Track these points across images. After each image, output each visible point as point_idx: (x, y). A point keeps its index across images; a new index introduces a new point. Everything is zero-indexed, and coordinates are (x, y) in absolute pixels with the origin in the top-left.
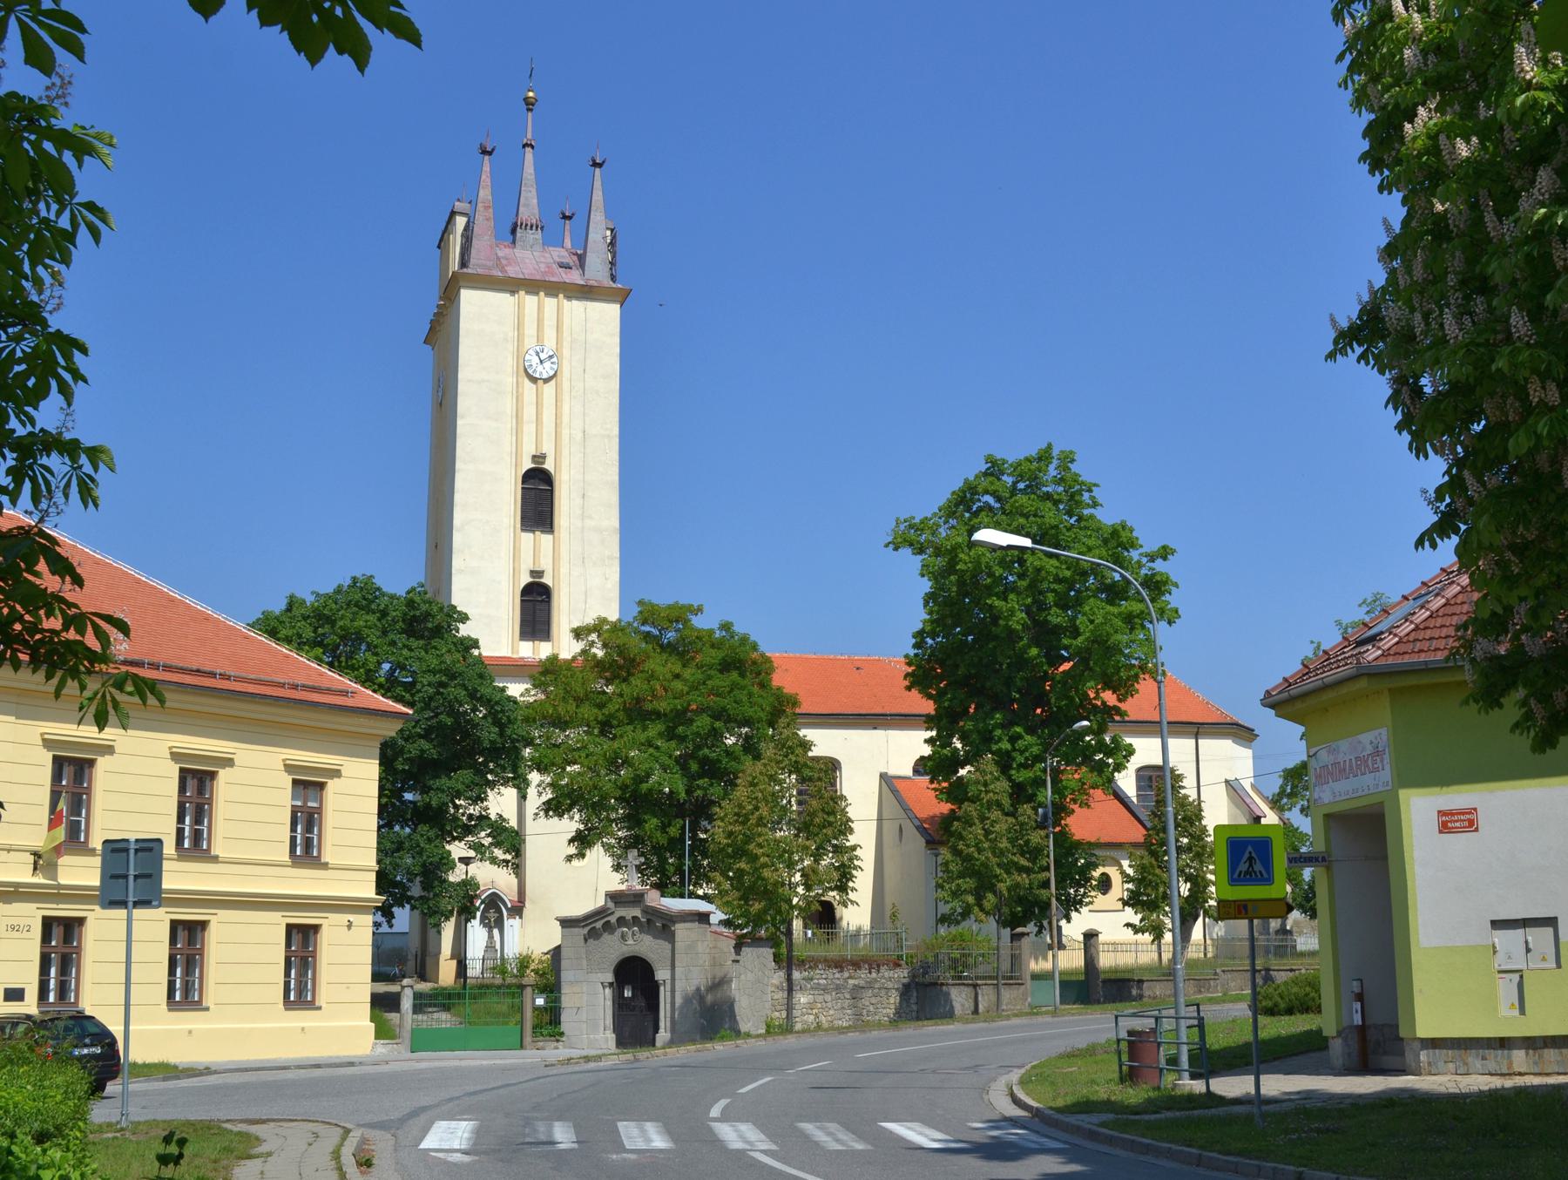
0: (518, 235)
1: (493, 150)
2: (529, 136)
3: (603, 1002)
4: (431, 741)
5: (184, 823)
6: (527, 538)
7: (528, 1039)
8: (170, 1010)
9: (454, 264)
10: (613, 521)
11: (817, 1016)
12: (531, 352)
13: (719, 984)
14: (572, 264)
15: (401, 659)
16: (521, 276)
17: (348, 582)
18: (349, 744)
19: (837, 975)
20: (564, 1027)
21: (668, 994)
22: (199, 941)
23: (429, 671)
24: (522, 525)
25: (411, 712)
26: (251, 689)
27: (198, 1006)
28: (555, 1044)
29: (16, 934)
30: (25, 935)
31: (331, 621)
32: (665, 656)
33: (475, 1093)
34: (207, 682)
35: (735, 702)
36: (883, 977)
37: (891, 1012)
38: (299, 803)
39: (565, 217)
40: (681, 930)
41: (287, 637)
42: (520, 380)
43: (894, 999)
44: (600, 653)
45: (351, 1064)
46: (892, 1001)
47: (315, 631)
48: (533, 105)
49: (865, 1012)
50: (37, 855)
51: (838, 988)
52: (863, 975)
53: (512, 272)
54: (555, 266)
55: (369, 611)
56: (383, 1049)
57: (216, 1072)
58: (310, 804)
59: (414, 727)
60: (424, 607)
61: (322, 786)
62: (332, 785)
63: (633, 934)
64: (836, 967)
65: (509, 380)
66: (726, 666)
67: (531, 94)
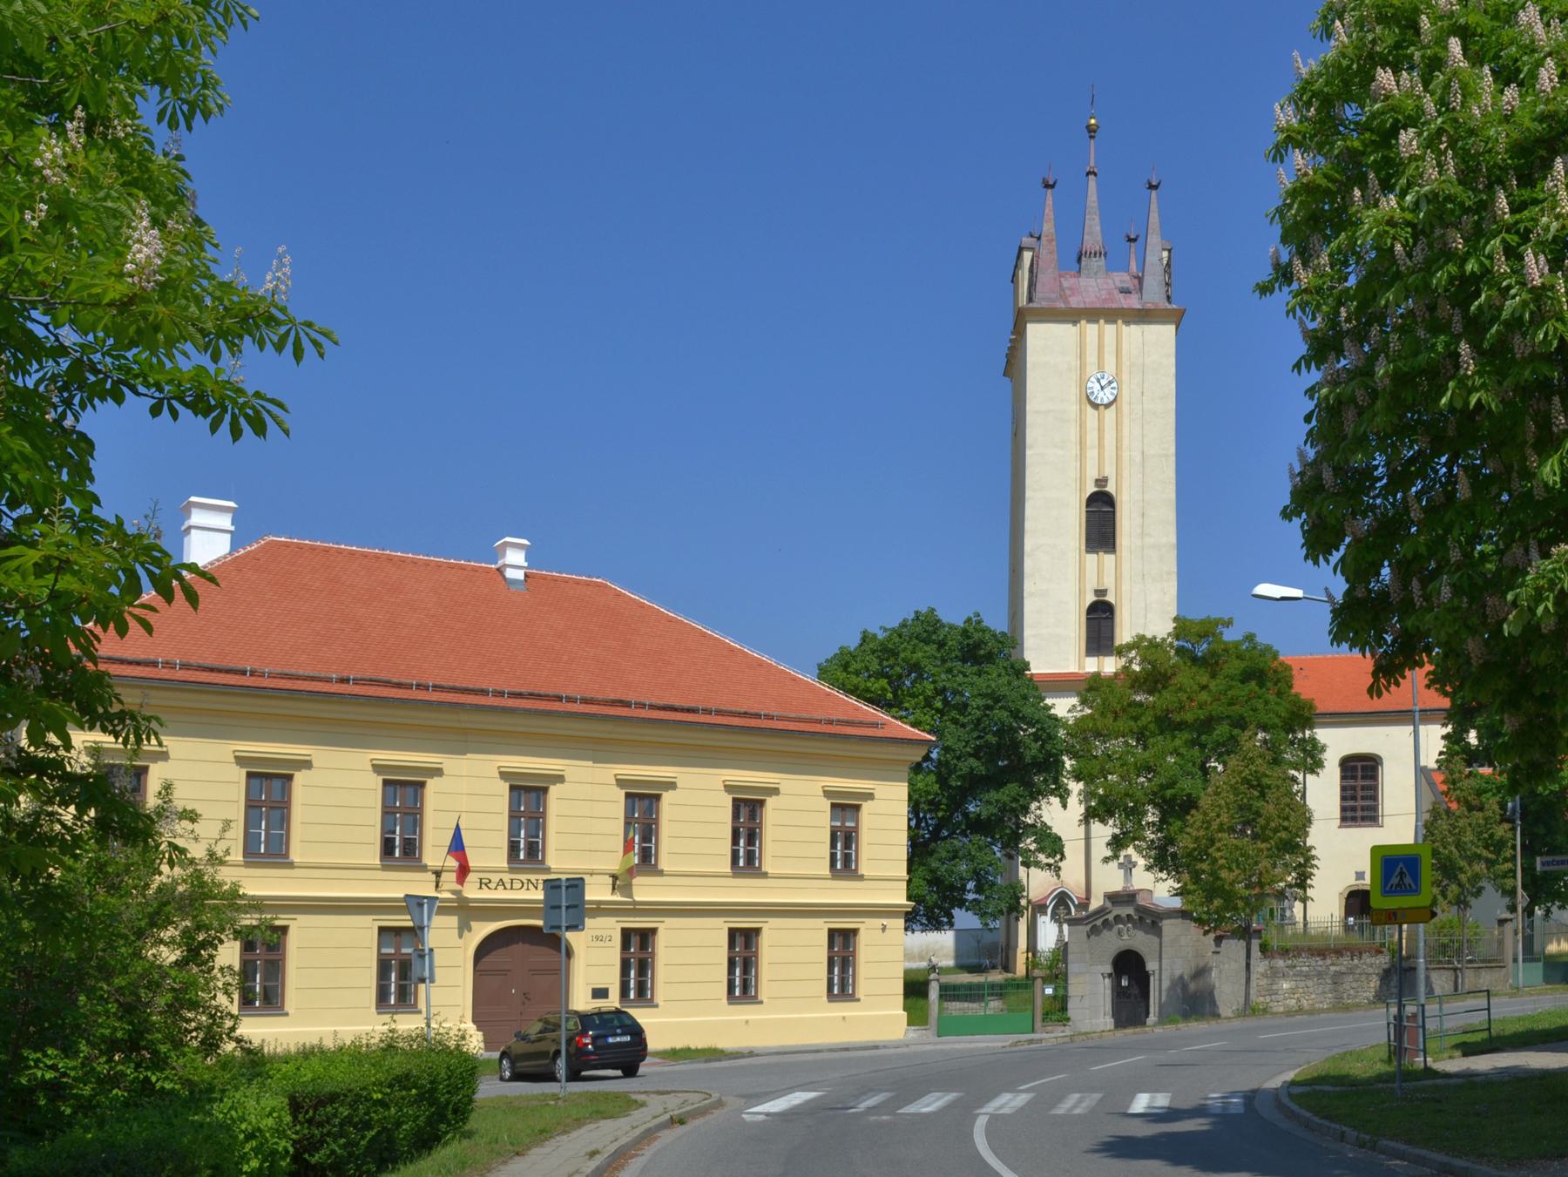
0: (1083, 263)
1: (1055, 183)
2: (1092, 164)
3: (1104, 988)
4: (979, 758)
5: (738, 844)
6: (1092, 558)
7: (1038, 1024)
8: (829, 1001)
9: (1023, 300)
10: (1171, 537)
11: (1298, 1000)
12: (1093, 379)
13: (1201, 972)
14: (1132, 288)
15: (955, 685)
16: (1082, 306)
17: (912, 616)
18: (881, 770)
19: (1320, 963)
20: (1070, 1013)
21: (1157, 982)
22: (754, 945)
23: (980, 695)
24: (1087, 546)
25: (934, 739)
26: (792, 726)
27: (755, 1000)
28: (1063, 1028)
29: (602, 944)
30: (608, 944)
31: (895, 654)
32: (1194, 669)
33: (876, 1071)
34: (753, 723)
35: (1252, 710)
36: (1365, 963)
37: (1371, 995)
38: (839, 824)
39: (1130, 240)
40: (1167, 926)
41: (856, 670)
42: (1083, 407)
43: (1375, 983)
44: (1137, 668)
45: (876, 1047)
46: (1372, 985)
47: (880, 664)
48: (1095, 132)
49: (1345, 996)
50: (615, 877)
51: (1320, 975)
52: (1345, 961)
53: (1075, 302)
54: (1116, 292)
55: (927, 642)
56: (914, 1034)
57: (757, 1055)
58: (848, 824)
59: (964, 747)
60: (977, 636)
61: (857, 808)
62: (867, 807)
63: (1128, 930)
64: (1319, 955)
65: (1073, 408)
66: (1246, 677)
67: (1093, 121)
